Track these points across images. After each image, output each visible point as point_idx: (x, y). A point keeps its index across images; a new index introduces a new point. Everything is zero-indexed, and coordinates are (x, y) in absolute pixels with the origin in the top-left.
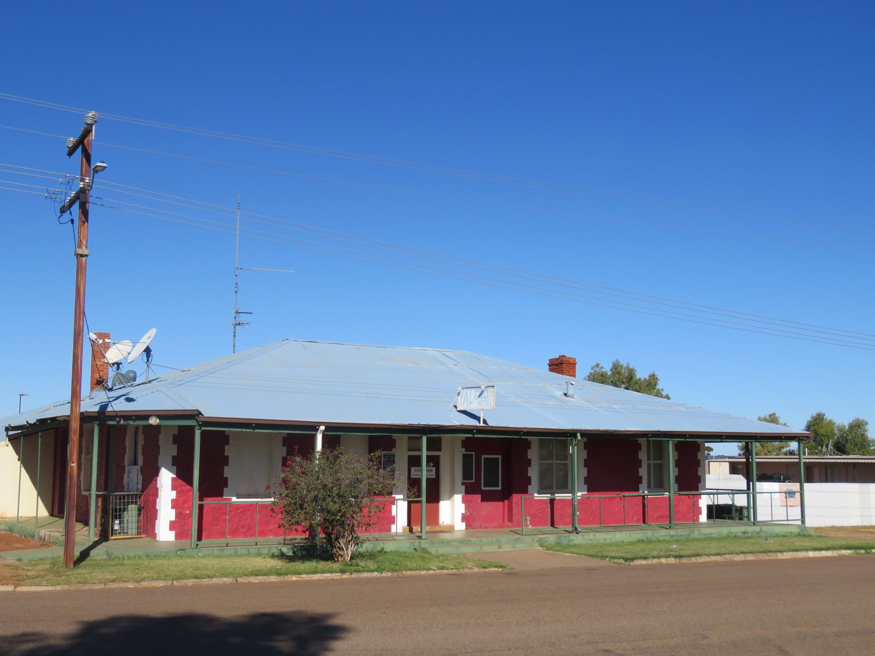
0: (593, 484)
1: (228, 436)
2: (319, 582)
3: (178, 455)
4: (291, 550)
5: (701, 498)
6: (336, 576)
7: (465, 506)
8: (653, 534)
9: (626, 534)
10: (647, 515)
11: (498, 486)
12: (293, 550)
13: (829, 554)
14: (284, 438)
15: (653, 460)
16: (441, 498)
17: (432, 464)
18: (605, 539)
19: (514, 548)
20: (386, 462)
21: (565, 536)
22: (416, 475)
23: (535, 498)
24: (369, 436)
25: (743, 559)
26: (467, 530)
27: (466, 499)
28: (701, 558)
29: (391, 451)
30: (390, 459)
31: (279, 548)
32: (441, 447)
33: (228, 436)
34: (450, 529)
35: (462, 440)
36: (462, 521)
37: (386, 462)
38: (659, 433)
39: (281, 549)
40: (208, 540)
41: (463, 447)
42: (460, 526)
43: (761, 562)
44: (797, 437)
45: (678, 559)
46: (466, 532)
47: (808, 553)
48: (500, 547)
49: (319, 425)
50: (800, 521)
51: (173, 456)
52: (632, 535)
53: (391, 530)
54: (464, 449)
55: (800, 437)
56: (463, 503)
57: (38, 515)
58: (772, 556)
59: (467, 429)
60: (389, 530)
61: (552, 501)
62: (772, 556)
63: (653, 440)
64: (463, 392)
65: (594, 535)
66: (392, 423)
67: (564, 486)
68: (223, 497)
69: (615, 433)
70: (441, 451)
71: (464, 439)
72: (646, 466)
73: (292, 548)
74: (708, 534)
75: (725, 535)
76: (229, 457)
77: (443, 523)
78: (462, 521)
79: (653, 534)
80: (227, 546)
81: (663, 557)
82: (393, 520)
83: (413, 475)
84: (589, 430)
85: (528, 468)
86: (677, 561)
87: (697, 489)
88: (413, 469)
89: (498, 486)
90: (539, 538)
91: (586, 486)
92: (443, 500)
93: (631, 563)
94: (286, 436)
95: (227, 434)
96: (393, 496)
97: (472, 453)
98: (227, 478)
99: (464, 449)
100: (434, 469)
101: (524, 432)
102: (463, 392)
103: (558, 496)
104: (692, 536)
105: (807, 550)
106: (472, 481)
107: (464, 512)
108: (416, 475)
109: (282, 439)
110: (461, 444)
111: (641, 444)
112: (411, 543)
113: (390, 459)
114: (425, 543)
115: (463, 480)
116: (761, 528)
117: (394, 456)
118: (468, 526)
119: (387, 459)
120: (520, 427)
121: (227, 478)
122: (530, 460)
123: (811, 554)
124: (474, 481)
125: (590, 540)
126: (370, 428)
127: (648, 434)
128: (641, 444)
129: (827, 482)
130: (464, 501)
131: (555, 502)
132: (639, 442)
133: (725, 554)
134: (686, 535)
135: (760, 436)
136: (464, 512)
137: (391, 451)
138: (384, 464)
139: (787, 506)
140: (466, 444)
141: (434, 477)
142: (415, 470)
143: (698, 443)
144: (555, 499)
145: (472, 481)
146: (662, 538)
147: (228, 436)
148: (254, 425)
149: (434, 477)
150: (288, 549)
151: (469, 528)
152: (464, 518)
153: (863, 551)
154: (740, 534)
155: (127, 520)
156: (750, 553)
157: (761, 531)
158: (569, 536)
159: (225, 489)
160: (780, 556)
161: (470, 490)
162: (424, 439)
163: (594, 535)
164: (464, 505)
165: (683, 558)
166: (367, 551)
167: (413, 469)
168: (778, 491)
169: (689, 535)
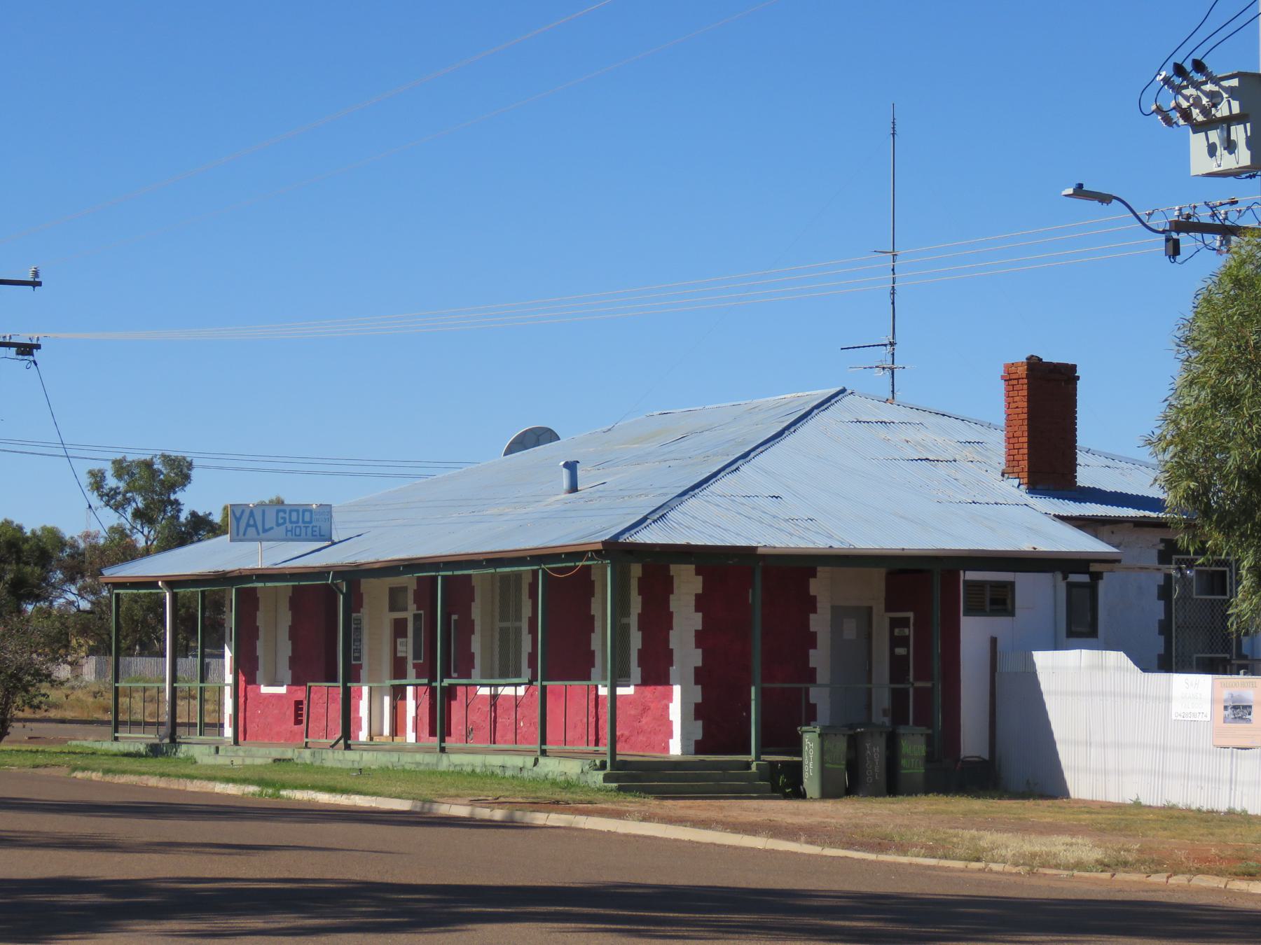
24: (293, 586)
29: (359, 612)
56: (639, 666)
57: (465, 689)
64: (1200, 802)
76: (694, 646)
88: (399, 640)
98: (672, 650)
102: (1200, 802)
109: (693, 634)
111: (816, 633)
117: (360, 620)
121: (672, 650)
128: (816, 633)
139: (174, 725)
141: (398, 640)
149: (398, 640)
155: (19, 767)
159: (1163, 618)
167: (399, 640)
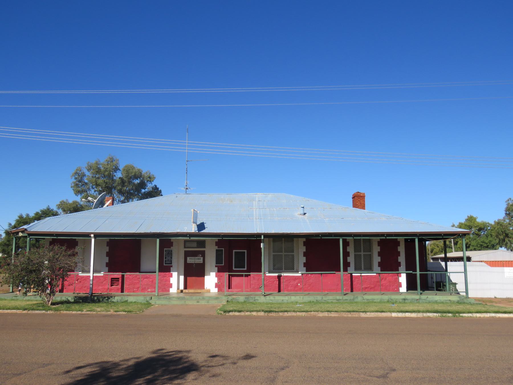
0: (309, 267)
1: (77, 242)
2: (37, 314)
3: (109, 252)
4: (73, 299)
5: (401, 276)
6: (19, 311)
7: (218, 279)
8: (322, 298)
9: (300, 297)
10: (354, 286)
11: (245, 268)
12: (74, 299)
13: (414, 315)
14: (378, 242)
15: (284, 252)
16: (205, 274)
17: (201, 255)
18: (283, 300)
19: (208, 303)
20: (167, 254)
21: (252, 297)
22: (191, 261)
23: (79, 275)
25: (327, 315)
26: (219, 292)
27: (218, 275)
28: (288, 314)
29: (170, 248)
30: (169, 253)
31: (67, 298)
32: (205, 246)
33: (78, 242)
34: (209, 291)
35: (216, 242)
36: (216, 287)
37: (167, 254)
38: (327, 234)
39: (68, 298)
40: (67, 293)
41: (216, 245)
42: (215, 290)
43: (347, 318)
44: (457, 234)
45: (267, 313)
46: (218, 293)
47: (391, 314)
48: (198, 302)
49: (90, 234)
50: (465, 293)
51: (378, 252)
52: (304, 298)
53: (170, 291)
54: (217, 247)
55: (459, 234)
58: (356, 315)
59: (183, 235)
60: (169, 291)
61: (279, 277)
62: (356, 315)
63: (363, 239)
65: (274, 297)
66: (277, 232)
67: (291, 268)
68: (170, 272)
69: (291, 235)
70: (205, 248)
71: (51, 240)
72: (354, 256)
73: (74, 298)
74: (371, 299)
75: (386, 301)
77: (207, 288)
78: (216, 287)
79: (322, 298)
80: (436, 295)
81: (255, 311)
82: (171, 286)
83: (188, 261)
84: (268, 233)
85: (398, 257)
86: (266, 314)
87: (398, 270)
89: (245, 268)
90: (233, 297)
91: (305, 268)
92: (206, 276)
93: (227, 314)
94: (379, 240)
95: (77, 240)
96: (171, 273)
97: (223, 249)
99: (217, 247)
100: (202, 258)
101: (222, 235)
103: (284, 274)
104: (356, 300)
105: (391, 312)
106: (164, 264)
107: (217, 282)
108: (197, 261)
109: (106, 243)
110: (215, 244)
112: (144, 298)
113: (169, 253)
114: (154, 298)
115: (216, 264)
116: (420, 297)
117: (172, 251)
118: (219, 290)
119: (167, 253)
120: (331, 232)
122: (399, 252)
123: (394, 315)
124: (223, 265)
125: (271, 300)
126: (313, 235)
127: (319, 235)
129: (496, 267)
130: (216, 276)
131: (281, 278)
132: (347, 241)
133: (311, 311)
134: (350, 300)
135: (419, 234)
136: (217, 282)
137: (170, 248)
138: (165, 255)
140: (218, 244)
141: (202, 262)
142: (190, 259)
143: (172, 241)
144: (281, 276)
145: (164, 264)
146: (330, 301)
147: (78, 242)
148: (55, 235)
149: (202, 262)
150: (72, 298)
151: (220, 291)
152: (217, 286)
153: (450, 315)
154: (401, 301)
156: (336, 311)
157: (420, 299)
158: (254, 298)
160: (363, 315)
161: (220, 270)
162: (158, 240)
163: (274, 297)
164: (217, 278)
165: (476, 311)
166: (117, 301)
168: (402, 274)
169: (353, 299)
